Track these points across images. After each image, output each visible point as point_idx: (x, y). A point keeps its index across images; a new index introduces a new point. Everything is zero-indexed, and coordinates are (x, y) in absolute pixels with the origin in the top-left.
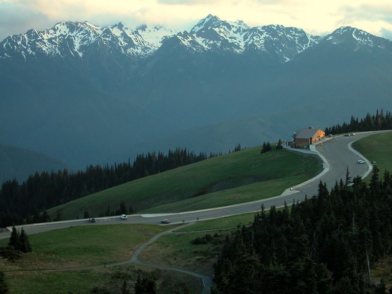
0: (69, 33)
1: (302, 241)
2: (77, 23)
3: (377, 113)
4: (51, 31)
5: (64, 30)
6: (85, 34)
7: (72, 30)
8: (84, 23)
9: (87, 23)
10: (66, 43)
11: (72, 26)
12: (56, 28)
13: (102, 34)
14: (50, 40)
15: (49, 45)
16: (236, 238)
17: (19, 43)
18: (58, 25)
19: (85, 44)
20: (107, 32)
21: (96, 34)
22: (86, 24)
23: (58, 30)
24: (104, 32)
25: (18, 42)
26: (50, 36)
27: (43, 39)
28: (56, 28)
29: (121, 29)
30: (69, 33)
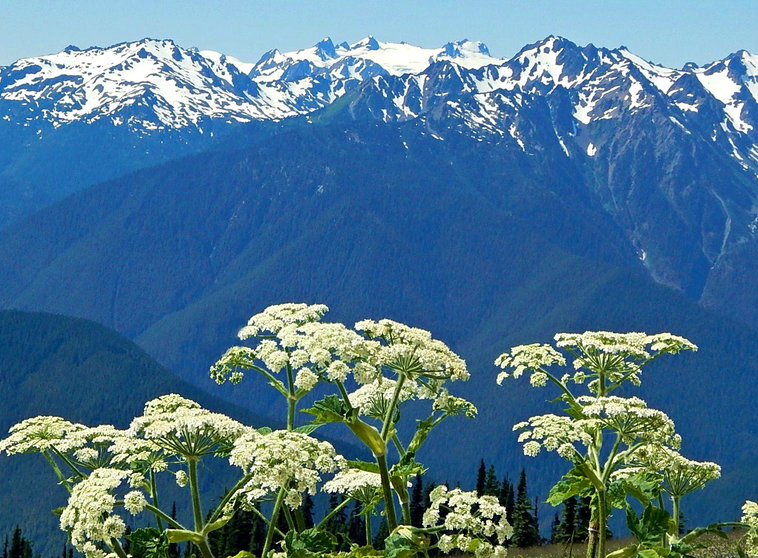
0: (560, 79)
1: (565, 453)
2: (592, 50)
3: (195, 88)
4: (507, 72)
5: (549, 64)
6: (612, 85)
7: (571, 70)
8: (615, 51)
9: (624, 53)
10: (545, 110)
11: (572, 56)
12: (522, 61)
13: (670, 90)
14: (495, 96)
15: (489, 112)
16: (557, 542)
17: (399, 101)
18: (528, 54)
19: (606, 117)
20: (689, 84)
21: (649, 88)
22: (620, 55)
23: (528, 69)
24: (676, 83)
25: (395, 100)
26: (498, 85)
27: (476, 92)
28: (522, 61)
29: (739, 81)
30: (560, 79)
